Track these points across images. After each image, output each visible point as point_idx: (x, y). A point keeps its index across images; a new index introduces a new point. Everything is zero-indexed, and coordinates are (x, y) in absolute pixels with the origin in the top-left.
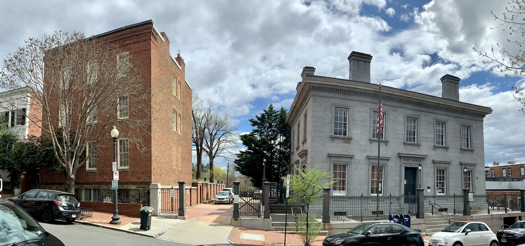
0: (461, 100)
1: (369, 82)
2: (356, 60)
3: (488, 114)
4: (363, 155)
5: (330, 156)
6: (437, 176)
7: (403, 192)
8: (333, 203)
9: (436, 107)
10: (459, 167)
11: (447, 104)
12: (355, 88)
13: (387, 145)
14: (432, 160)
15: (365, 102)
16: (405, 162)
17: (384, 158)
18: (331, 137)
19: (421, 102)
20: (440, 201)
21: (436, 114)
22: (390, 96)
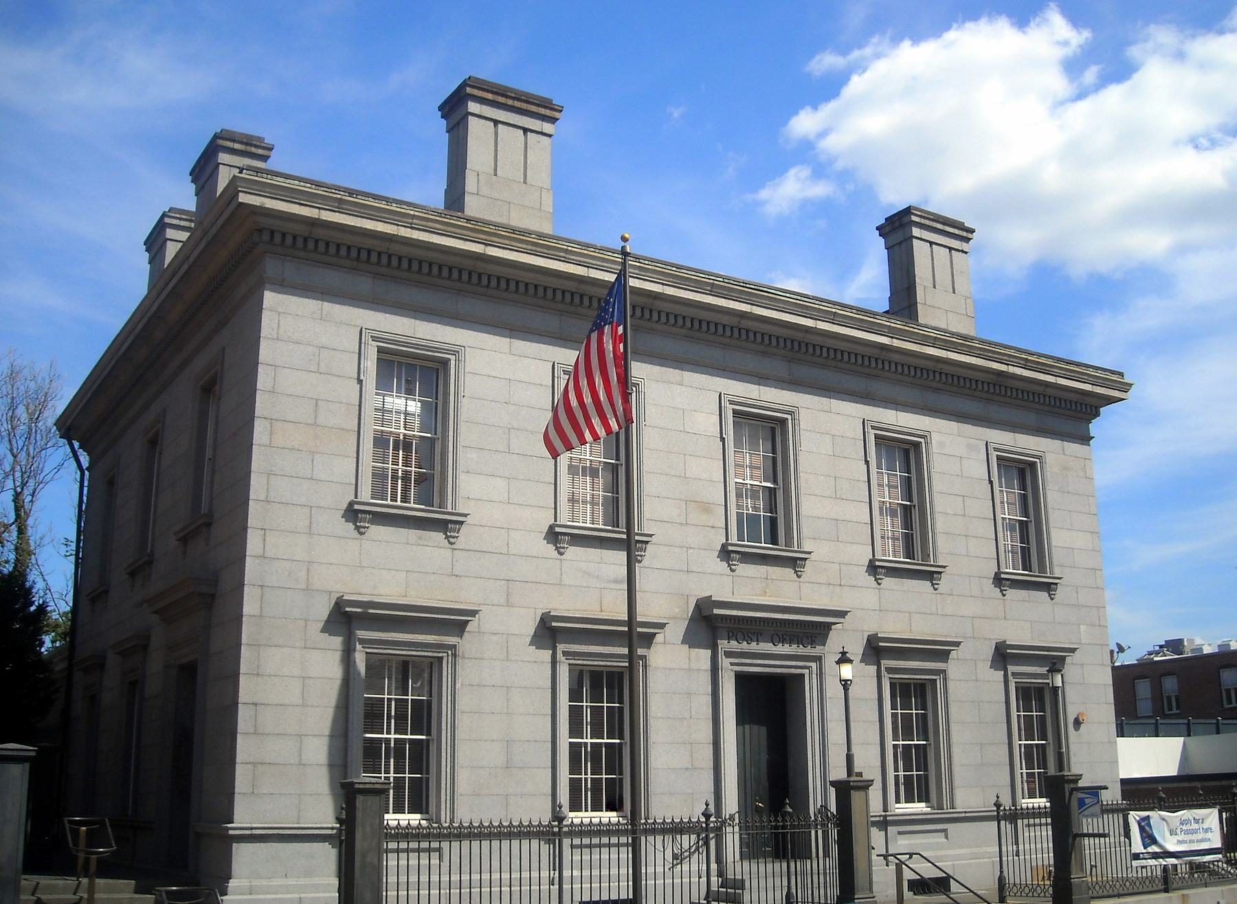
16: (734, 645)
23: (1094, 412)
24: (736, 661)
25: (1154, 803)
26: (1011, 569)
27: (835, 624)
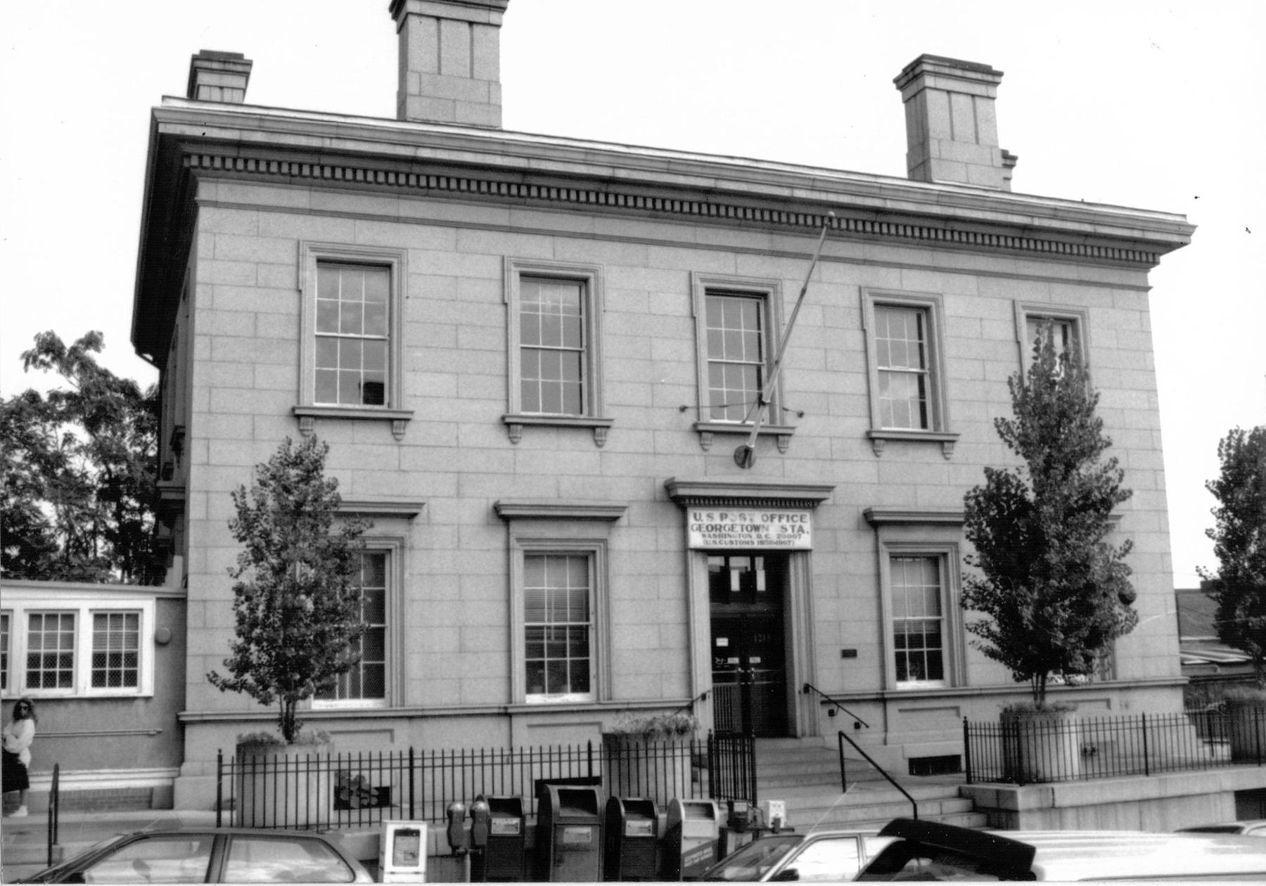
1: (494, 123)
3: (1170, 247)
7: (704, 680)
12: (837, 203)
13: (599, 444)
22: (516, 179)
23: (1151, 259)
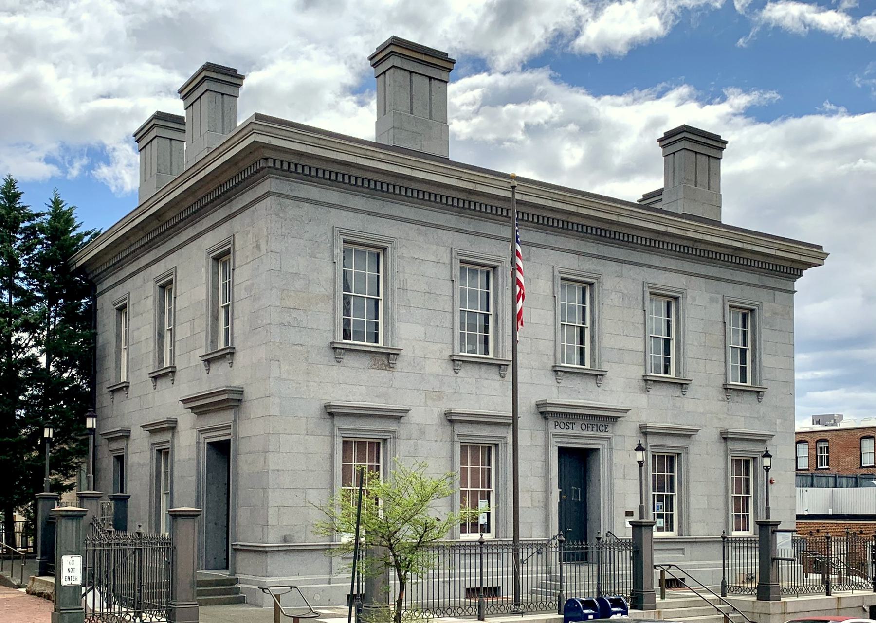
0: (729, 216)
1: (445, 155)
2: (402, 72)
3: (811, 265)
4: (432, 410)
5: (331, 414)
6: (464, 471)
7: (555, 530)
8: (463, 562)
9: (391, 188)
10: (718, 448)
11: (690, 235)
14: (638, 424)
15: (438, 227)
16: (558, 431)
17: (672, 432)
18: (334, 348)
19: (606, 226)
20: (664, 556)
21: (650, 266)
22: (463, 196)
24: (559, 440)
25: (573, 544)
26: (735, 382)
27: (620, 417)
